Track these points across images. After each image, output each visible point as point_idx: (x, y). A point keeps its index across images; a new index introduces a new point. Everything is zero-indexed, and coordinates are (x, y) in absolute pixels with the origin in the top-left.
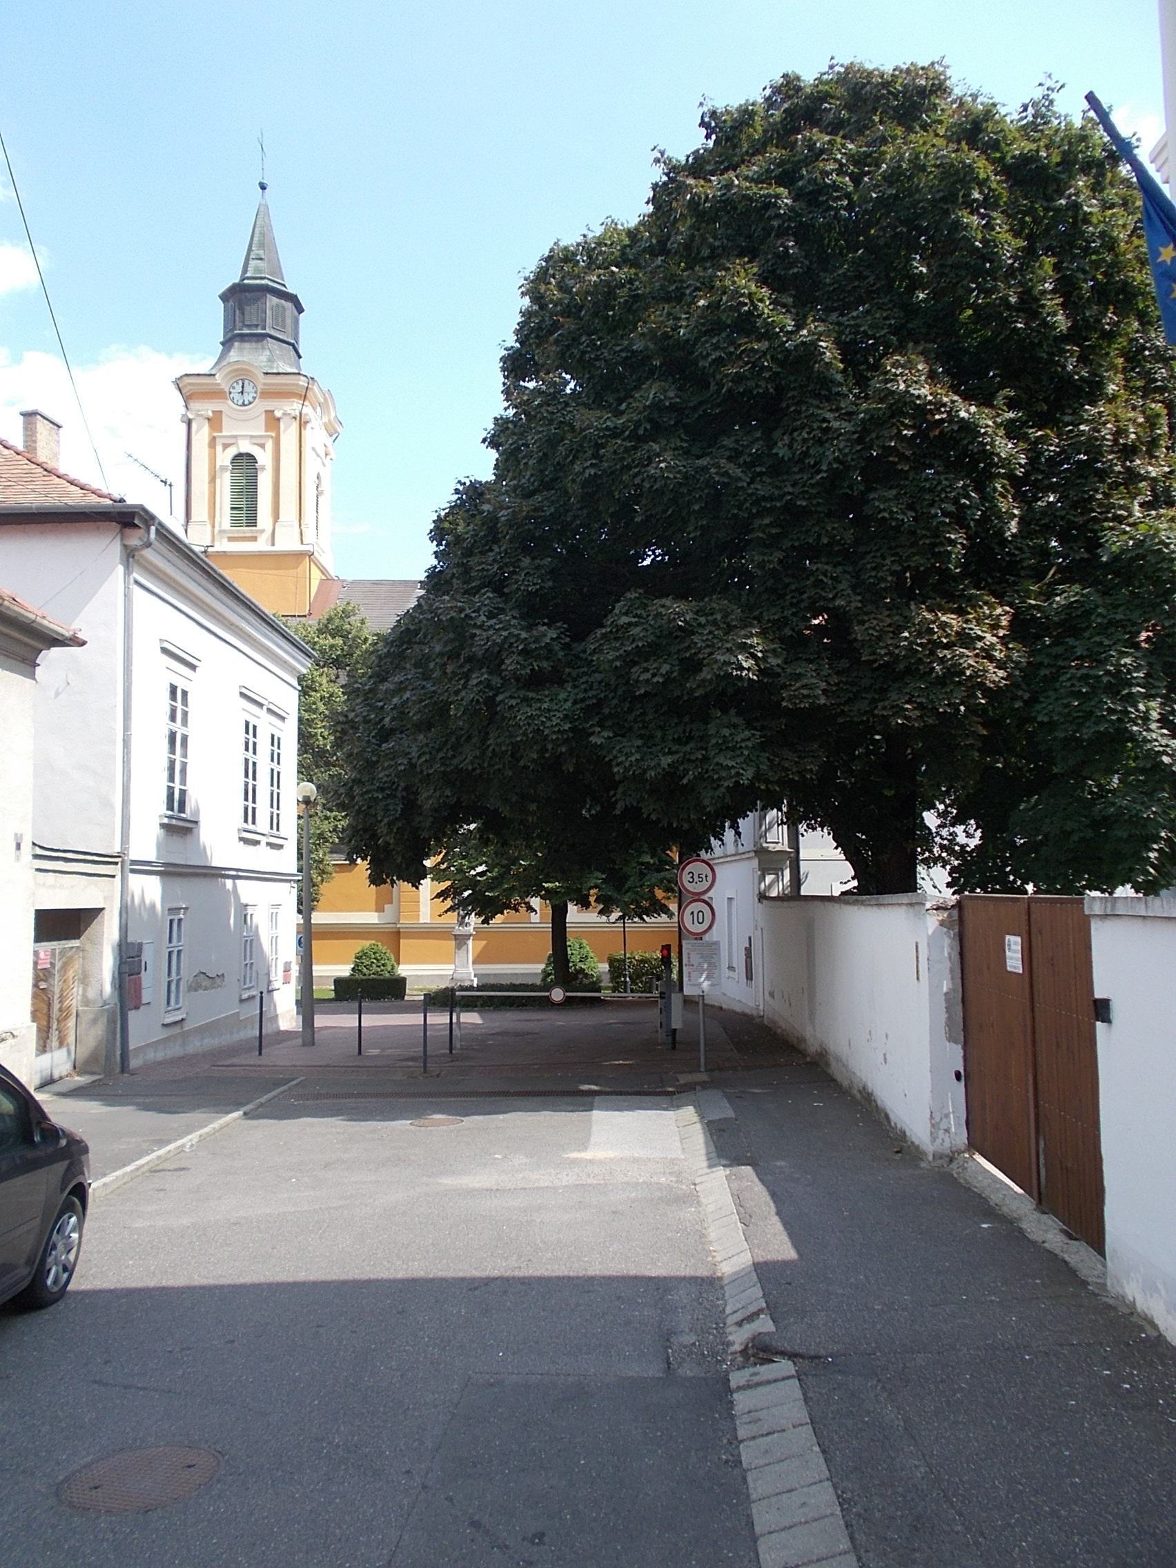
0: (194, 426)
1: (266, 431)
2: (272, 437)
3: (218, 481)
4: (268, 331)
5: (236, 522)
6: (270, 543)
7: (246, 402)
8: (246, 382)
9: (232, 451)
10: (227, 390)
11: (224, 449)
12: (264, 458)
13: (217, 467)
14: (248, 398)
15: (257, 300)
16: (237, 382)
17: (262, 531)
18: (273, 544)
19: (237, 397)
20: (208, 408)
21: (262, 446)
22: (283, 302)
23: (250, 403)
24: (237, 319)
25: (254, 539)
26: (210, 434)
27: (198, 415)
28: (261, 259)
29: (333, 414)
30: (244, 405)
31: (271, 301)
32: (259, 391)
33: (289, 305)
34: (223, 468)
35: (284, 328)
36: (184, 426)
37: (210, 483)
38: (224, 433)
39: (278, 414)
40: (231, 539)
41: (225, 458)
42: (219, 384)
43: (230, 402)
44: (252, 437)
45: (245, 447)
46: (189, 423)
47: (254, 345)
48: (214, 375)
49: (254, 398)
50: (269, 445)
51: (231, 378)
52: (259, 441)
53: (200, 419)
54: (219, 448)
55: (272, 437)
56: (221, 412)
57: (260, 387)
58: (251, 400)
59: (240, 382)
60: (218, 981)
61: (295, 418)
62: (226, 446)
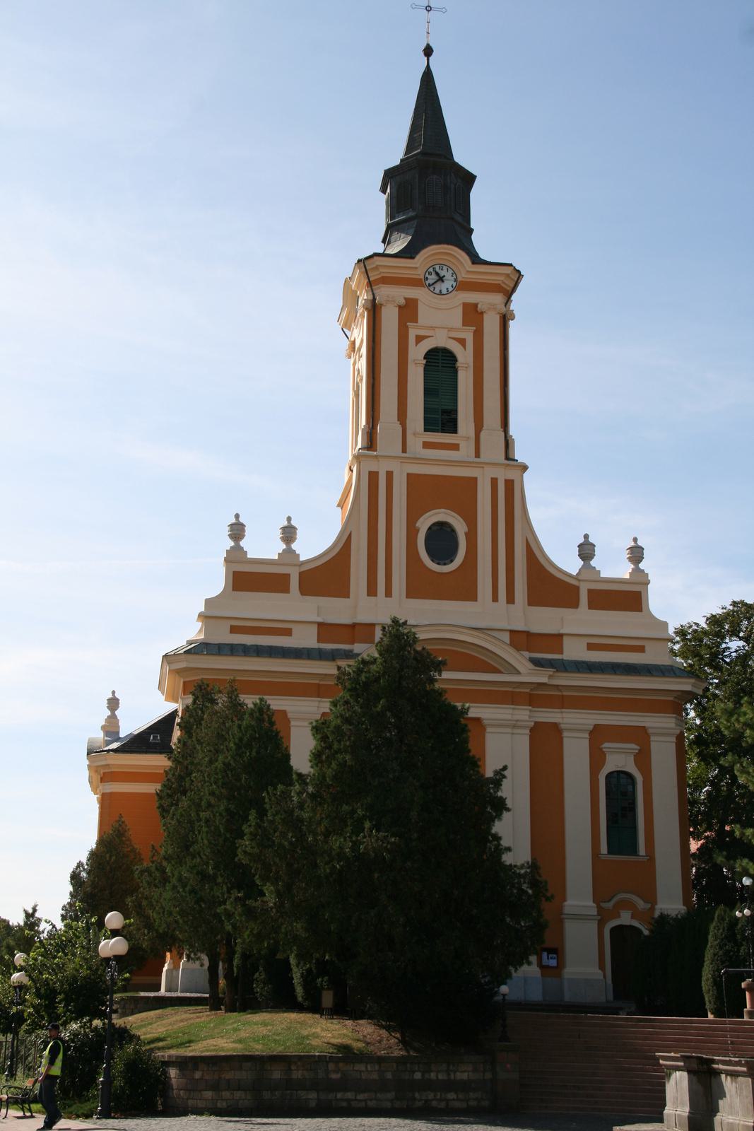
5: (429, 426)
12: (464, 357)
20: (401, 294)
21: (462, 342)
25: (455, 447)
40: (427, 445)
41: (417, 354)
45: (440, 340)
62: (419, 339)
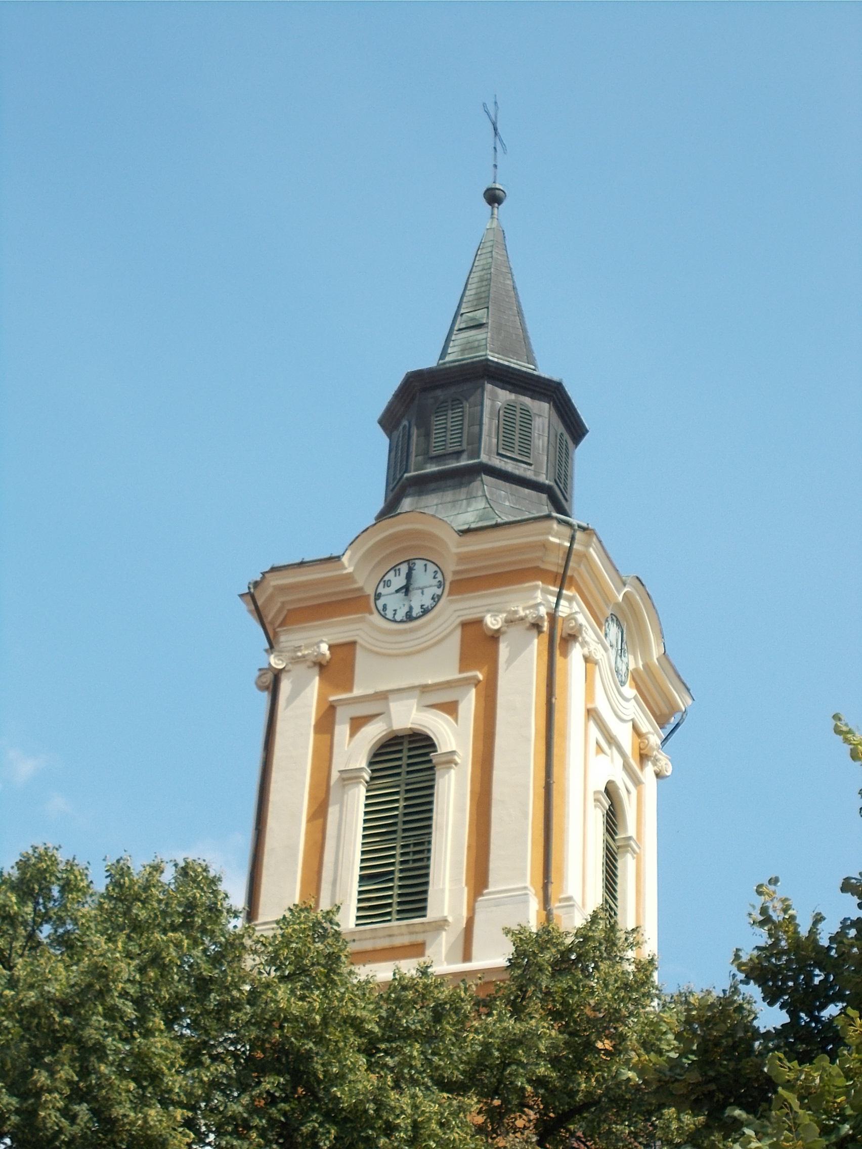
0: (285, 687)
1: (461, 671)
2: (477, 683)
3: (333, 812)
4: (484, 458)
6: (460, 953)
7: (416, 611)
8: (419, 565)
9: (374, 733)
10: (370, 591)
11: (354, 729)
13: (335, 775)
14: (418, 601)
15: (457, 402)
16: (395, 569)
17: (441, 925)
18: (467, 957)
19: (394, 603)
21: (451, 708)
22: (527, 400)
23: (425, 611)
24: (413, 448)
26: (322, 697)
27: (296, 660)
28: (480, 326)
29: (656, 652)
30: (409, 617)
31: (494, 398)
32: (449, 578)
33: (542, 410)
34: (349, 777)
35: (528, 454)
36: (265, 697)
37: (312, 818)
38: (357, 692)
39: (493, 622)
42: (349, 577)
43: (376, 618)
44: (425, 689)
46: (274, 689)
47: (449, 496)
48: (338, 558)
49: (436, 599)
50: (469, 703)
51: (379, 564)
52: (445, 697)
53: (300, 670)
54: (342, 730)
55: (477, 683)
56: (353, 644)
57: (450, 567)
58: (428, 602)
59: (404, 569)
60: (64, 1004)
61: (536, 626)
62: (357, 723)
